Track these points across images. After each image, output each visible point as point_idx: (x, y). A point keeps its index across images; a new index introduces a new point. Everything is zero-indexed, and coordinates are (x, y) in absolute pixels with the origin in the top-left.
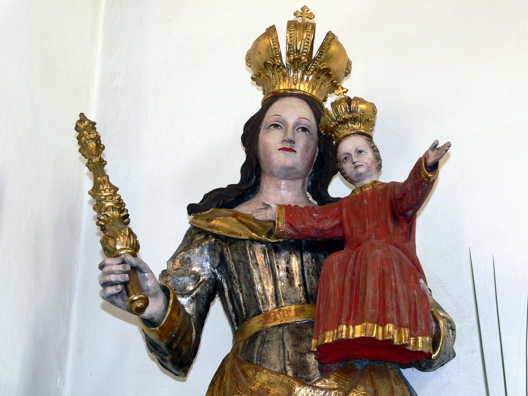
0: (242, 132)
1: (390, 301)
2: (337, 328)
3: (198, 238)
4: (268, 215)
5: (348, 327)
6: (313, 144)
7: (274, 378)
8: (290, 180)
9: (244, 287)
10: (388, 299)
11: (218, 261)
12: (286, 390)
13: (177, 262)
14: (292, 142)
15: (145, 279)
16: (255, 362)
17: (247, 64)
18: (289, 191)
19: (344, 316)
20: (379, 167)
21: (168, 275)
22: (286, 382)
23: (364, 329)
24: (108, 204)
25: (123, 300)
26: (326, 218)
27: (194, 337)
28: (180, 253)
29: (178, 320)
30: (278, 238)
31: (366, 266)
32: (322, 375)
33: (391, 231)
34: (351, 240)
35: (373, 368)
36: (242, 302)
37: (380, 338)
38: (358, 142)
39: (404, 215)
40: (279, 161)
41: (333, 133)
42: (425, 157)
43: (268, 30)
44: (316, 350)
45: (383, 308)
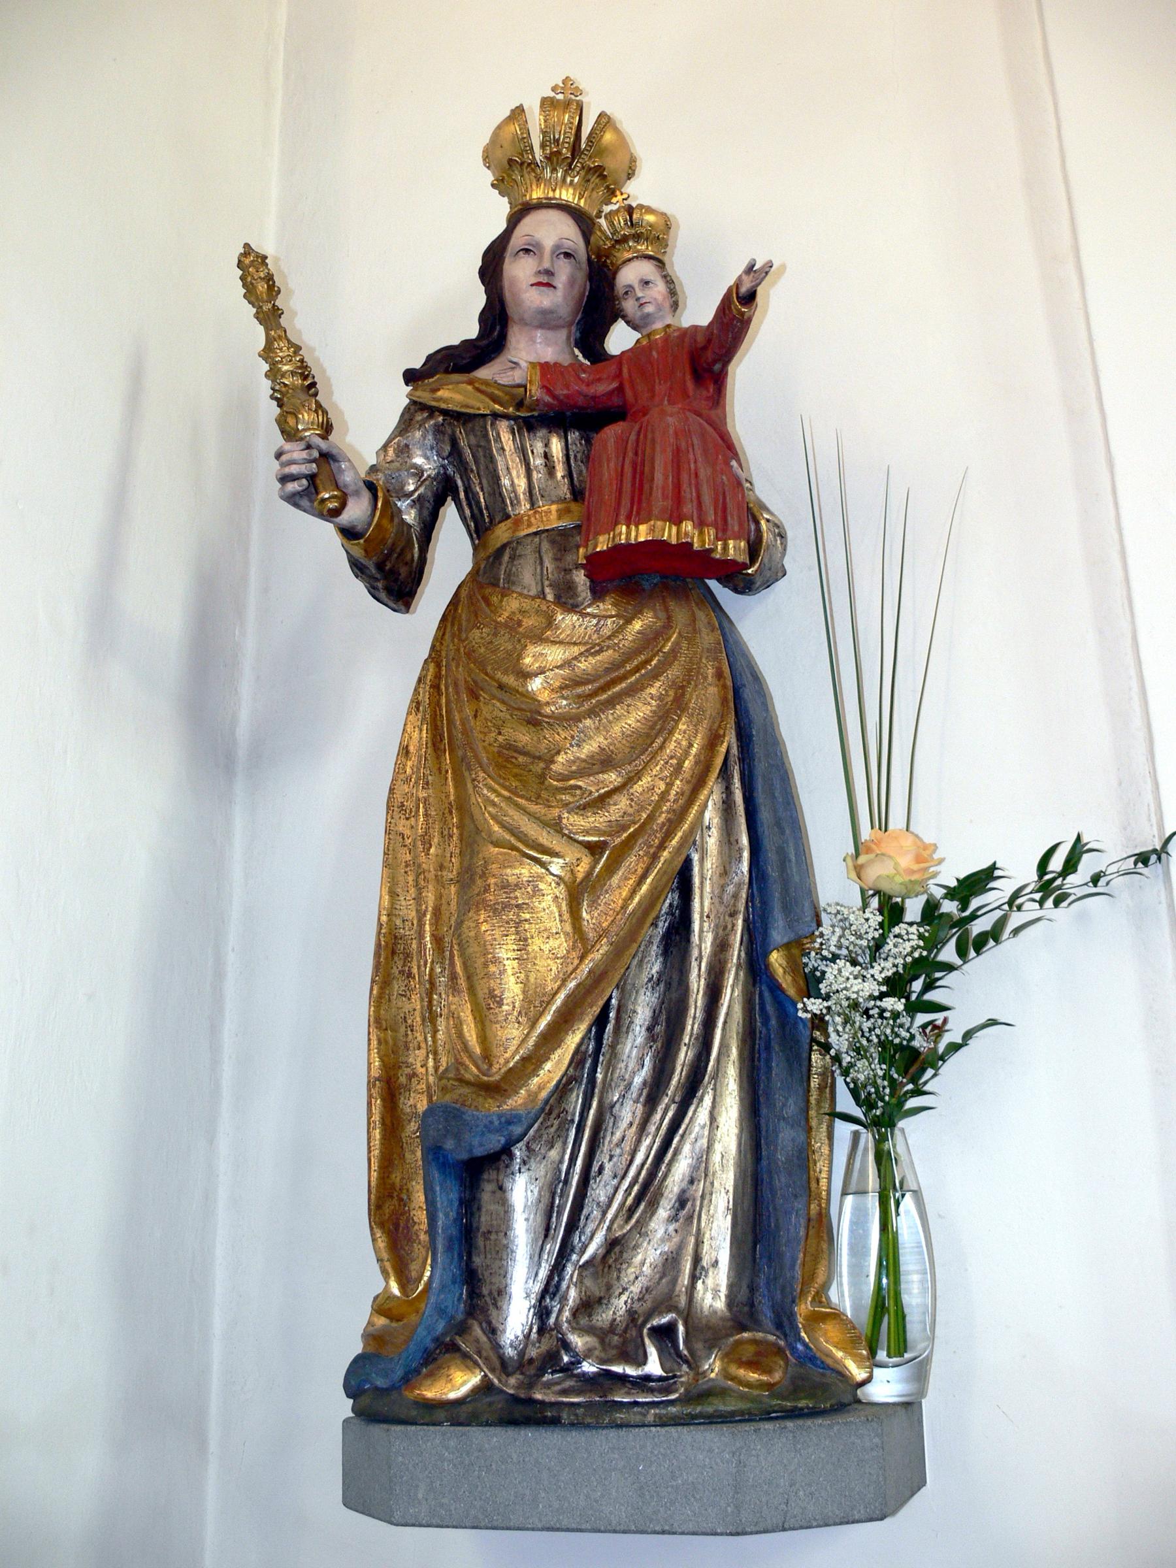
0: (480, 264)
1: (688, 490)
2: (614, 530)
3: (419, 417)
4: (517, 377)
5: (628, 527)
6: (581, 276)
7: (527, 604)
8: (549, 329)
9: (484, 482)
10: (685, 486)
11: (447, 448)
12: (544, 621)
13: (391, 452)
14: (549, 273)
15: (341, 471)
16: (501, 585)
17: (485, 165)
18: (548, 345)
19: (623, 512)
20: (675, 306)
21: (377, 471)
22: (544, 608)
23: (651, 530)
24: (285, 368)
25: (312, 501)
26: (599, 380)
27: (416, 555)
28: (394, 439)
29: (391, 530)
30: (532, 410)
31: (653, 440)
32: (594, 599)
33: (691, 393)
34: (634, 410)
35: (666, 587)
36: (483, 504)
37: (674, 541)
38: (645, 269)
39: (710, 370)
40: (531, 301)
41: (607, 257)
42: (738, 285)
43: (513, 111)
44: (585, 562)
45: (678, 499)
